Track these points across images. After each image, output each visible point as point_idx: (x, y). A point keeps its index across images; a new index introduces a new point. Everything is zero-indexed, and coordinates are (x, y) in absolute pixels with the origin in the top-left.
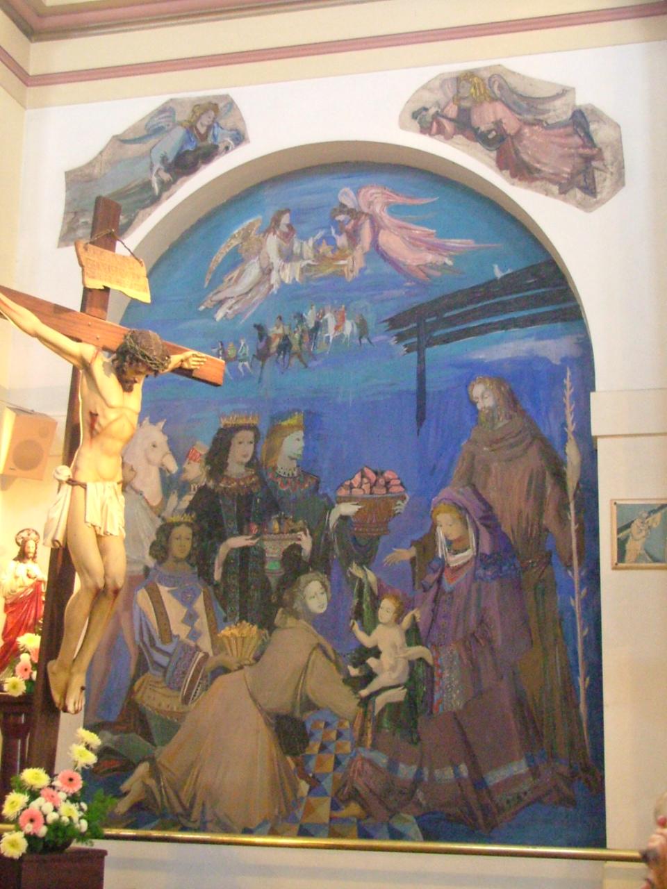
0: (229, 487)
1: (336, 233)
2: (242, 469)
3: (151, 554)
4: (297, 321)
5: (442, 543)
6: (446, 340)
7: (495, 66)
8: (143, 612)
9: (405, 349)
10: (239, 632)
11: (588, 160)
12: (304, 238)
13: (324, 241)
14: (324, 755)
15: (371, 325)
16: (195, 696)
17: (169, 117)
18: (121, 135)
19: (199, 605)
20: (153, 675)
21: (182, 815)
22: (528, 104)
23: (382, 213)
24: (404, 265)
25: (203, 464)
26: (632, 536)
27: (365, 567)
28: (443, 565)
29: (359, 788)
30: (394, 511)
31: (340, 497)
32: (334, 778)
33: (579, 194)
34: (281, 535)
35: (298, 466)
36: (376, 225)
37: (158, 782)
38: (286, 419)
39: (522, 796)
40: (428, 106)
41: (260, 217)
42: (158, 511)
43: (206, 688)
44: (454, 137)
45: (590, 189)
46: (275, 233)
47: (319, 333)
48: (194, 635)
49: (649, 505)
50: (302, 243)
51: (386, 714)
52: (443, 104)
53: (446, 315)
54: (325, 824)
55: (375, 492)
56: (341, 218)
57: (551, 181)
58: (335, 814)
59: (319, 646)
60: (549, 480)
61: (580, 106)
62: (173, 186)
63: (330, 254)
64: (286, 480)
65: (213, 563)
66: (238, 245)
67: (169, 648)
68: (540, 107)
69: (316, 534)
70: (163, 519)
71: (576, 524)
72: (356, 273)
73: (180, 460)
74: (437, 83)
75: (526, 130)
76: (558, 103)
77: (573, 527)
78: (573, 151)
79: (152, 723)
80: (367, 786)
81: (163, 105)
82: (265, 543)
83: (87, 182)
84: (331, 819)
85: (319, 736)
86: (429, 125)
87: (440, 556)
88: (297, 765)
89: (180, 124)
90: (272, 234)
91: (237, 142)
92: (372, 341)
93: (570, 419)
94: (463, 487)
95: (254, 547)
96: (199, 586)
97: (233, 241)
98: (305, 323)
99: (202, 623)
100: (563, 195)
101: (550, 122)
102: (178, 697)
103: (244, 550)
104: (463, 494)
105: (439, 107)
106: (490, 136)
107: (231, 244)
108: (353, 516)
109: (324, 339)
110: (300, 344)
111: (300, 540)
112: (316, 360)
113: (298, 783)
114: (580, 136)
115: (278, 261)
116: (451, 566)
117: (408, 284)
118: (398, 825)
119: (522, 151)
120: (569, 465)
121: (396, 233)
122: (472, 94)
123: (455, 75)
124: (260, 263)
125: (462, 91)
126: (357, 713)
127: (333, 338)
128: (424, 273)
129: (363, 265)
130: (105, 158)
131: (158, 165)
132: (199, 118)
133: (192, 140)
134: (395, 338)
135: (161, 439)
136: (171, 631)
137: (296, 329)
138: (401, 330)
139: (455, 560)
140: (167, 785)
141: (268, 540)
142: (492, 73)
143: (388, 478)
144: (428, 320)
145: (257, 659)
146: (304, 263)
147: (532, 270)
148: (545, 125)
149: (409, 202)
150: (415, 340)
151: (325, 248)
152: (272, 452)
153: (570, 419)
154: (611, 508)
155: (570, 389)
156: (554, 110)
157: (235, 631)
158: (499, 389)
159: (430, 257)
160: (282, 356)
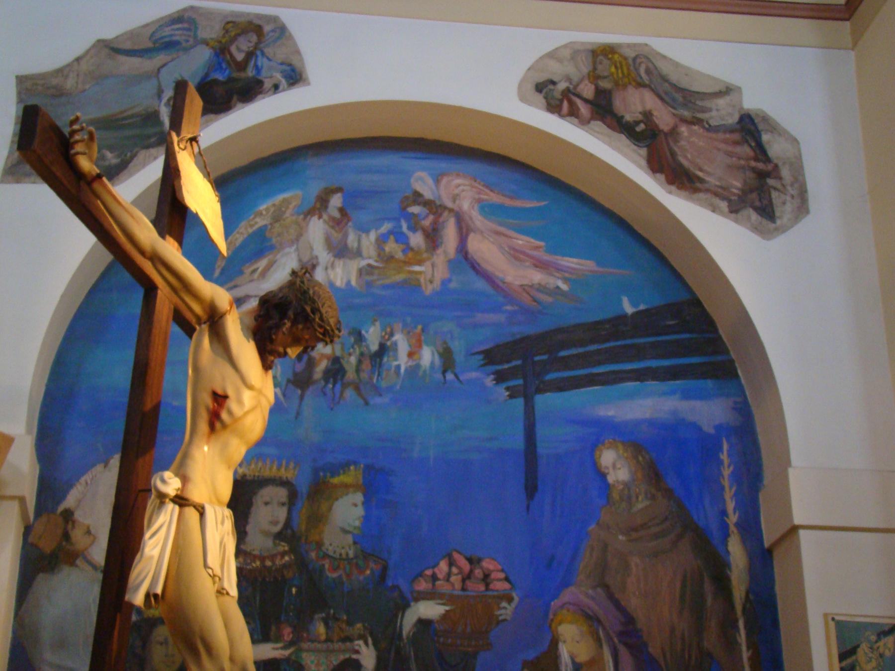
0: (248, 567)
1: (409, 228)
2: (269, 543)
4: (352, 340)
5: (567, 666)
6: (562, 386)
7: (640, 45)
9: (507, 393)
11: (762, 175)
12: (364, 229)
13: (392, 237)
15: (459, 357)
18: (111, 41)
22: (684, 97)
23: (472, 211)
24: (504, 283)
26: (860, 665)
30: (498, 616)
31: (419, 592)
33: (754, 216)
34: (329, 643)
35: (355, 543)
36: (464, 225)
38: (338, 474)
40: (555, 80)
41: (299, 192)
44: (592, 122)
45: (767, 212)
46: (320, 217)
47: (385, 359)
49: (878, 624)
52: (575, 79)
53: (563, 353)
55: (469, 588)
56: (415, 209)
57: (716, 194)
60: (708, 587)
61: (748, 110)
63: (399, 255)
64: (337, 561)
66: (266, 226)
68: (699, 103)
74: (567, 53)
75: (684, 129)
76: (721, 102)
78: (742, 162)
81: (178, 12)
82: (304, 655)
83: (53, 96)
86: (558, 103)
89: (206, 43)
91: (291, 81)
92: (461, 378)
93: (730, 506)
94: (594, 588)
95: (287, 660)
97: (258, 220)
98: (364, 344)
100: (733, 215)
101: (713, 123)
104: (593, 599)
105: (571, 83)
107: (256, 223)
108: (437, 621)
109: (393, 369)
110: (358, 370)
111: (357, 652)
112: (381, 395)
114: (750, 146)
117: (509, 308)
119: (679, 153)
121: (492, 240)
122: (612, 74)
123: (590, 47)
124: (298, 255)
125: (600, 67)
127: (406, 370)
128: (530, 295)
129: (447, 275)
130: (84, 66)
132: (233, 40)
133: (224, 66)
134: (492, 377)
137: (351, 350)
138: (499, 367)
141: (308, 651)
142: (637, 53)
143: (488, 570)
144: (537, 358)
146: (364, 263)
147: (674, 309)
148: (707, 126)
149: (507, 202)
150: (520, 382)
151: (391, 247)
152: (317, 519)
153: (730, 506)
156: (718, 110)
158: (636, 458)
159: (537, 277)
160: (330, 386)
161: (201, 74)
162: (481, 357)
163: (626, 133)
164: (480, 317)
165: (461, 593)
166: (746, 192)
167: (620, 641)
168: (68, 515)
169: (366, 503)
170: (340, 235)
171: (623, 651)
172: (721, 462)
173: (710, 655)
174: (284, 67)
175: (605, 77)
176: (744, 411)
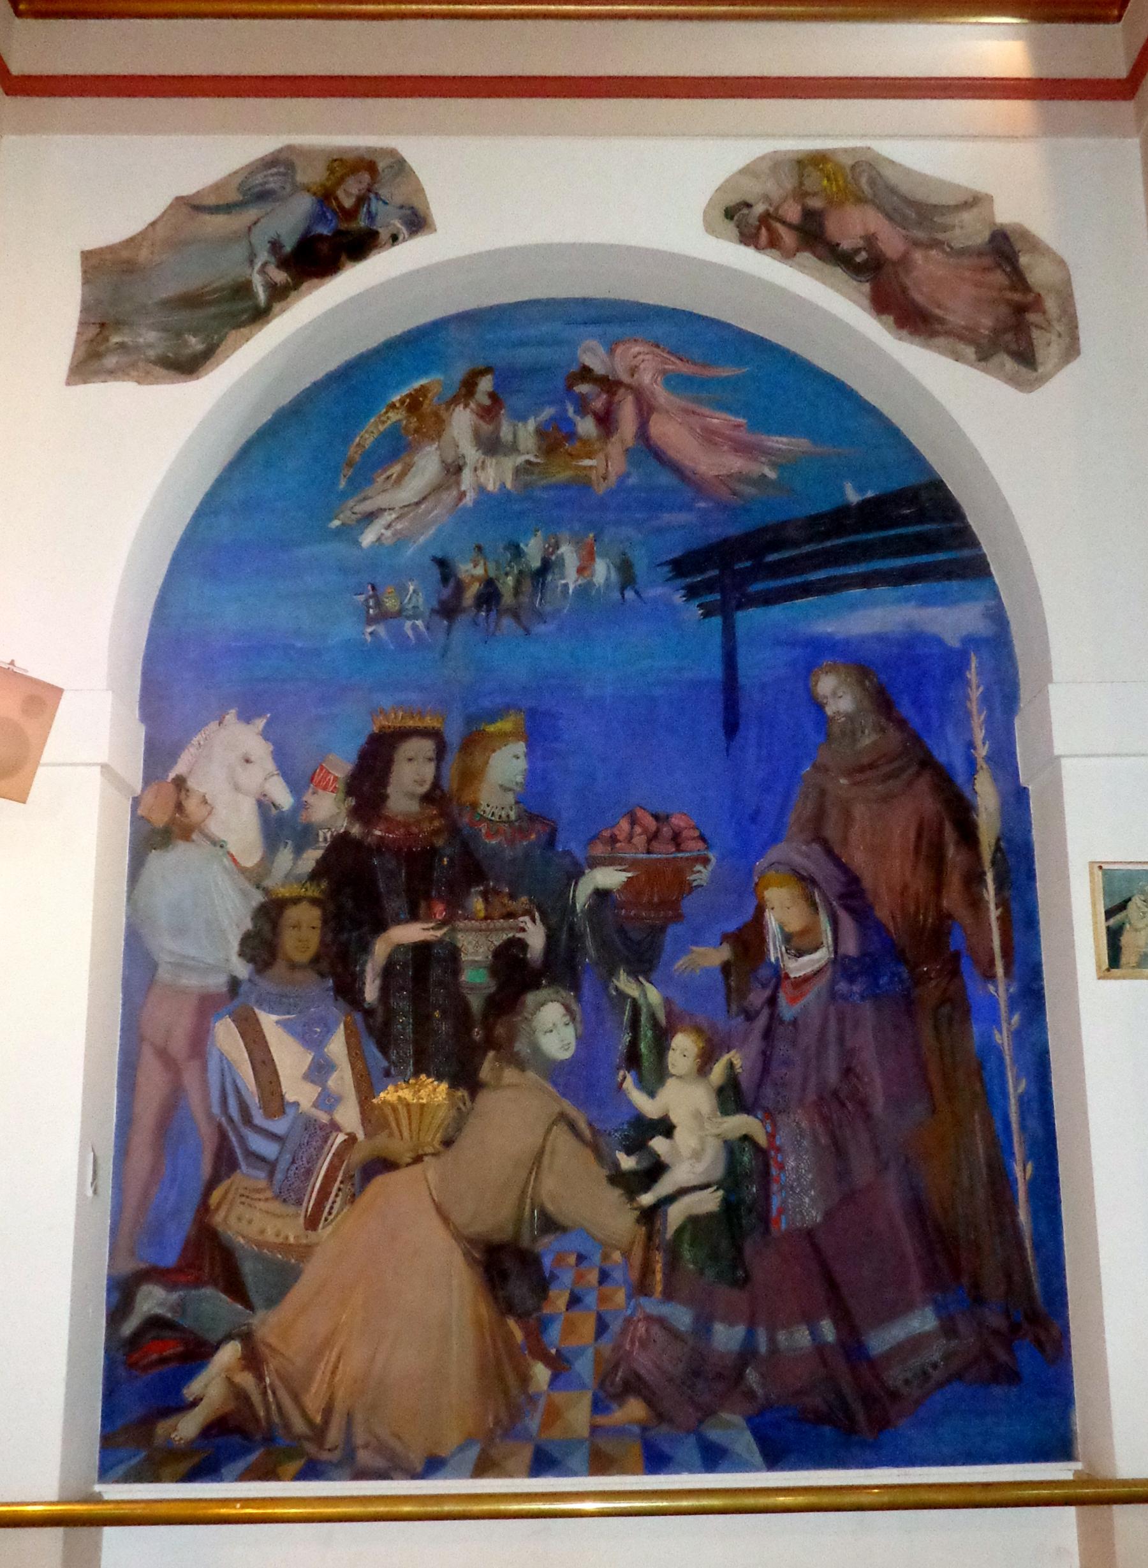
2: (414, 807)
3: (241, 954)
5: (775, 936)
6: (768, 599)
8: (228, 1062)
10: (413, 1095)
11: (1020, 310)
12: (521, 417)
14: (575, 1314)
15: (641, 566)
16: (330, 1213)
17: (284, 175)
19: (337, 1046)
20: (247, 1177)
21: (307, 1438)
25: (341, 795)
27: (641, 978)
28: (779, 976)
29: (642, 1372)
31: (594, 858)
32: (597, 1353)
33: (1010, 364)
35: (517, 803)
37: (260, 1378)
39: (930, 1370)
40: (750, 201)
42: (257, 877)
43: (353, 1198)
44: (798, 254)
45: (1026, 357)
46: (466, 406)
47: (549, 578)
48: (328, 1101)
50: (515, 426)
51: (687, 1237)
53: (772, 558)
54: (581, 1442)
56: (583, 388)
57: (961, 338)
58: (601, 1420)
59: (563, 1117)
60: (950, 834)
61: (1002, 225)
62: (293, 294)
64: (495, 826)
65: (363, 971)
66: (400, 421)
67: (279, 1126)
69: (554, 920)
70: (266, 891)
71: (997, 908)
72: (613, 479)
73: (296, 787)
75: (918, 256)
76: (966, 216)
77: (994, 913)
79: (248, 1268)
80: (658, 1368)
81: (272, 154)
82: (459, 936)
84: (594, 1429)
85: (567, 1278)
86: (754, 231)
87: (773, 959)
88: (527, 1335)
90: (462, 406)
91: (414, 229)
93: (979, 734)
94: (808, 843)
95: (440, 941)
96: (335, 1011)
99: (343, 1080)
100: (983, 364)
101: (957, 245)
102: (298, 1215)
103: (422, 950)
104: (808, 857)
105: (771, 205)
106: (858, 259)
108: (618, 890)
110: (517, 592)
111: (523, 930)
113: (529, 1366)
115: (473, 452)
116: (792, 976)
117: (702, 505)
118: (714, 1434)
120: (982, 809)
126: (635, 1237)
127: (575, 589)
130: (160, 231)
131: (263, 256)
132: (341, 180)
134: (682, 592)
135: (260, 749)
136: (282, 1097)
139: (798, 967)
140: (278, 1383)
141: (466, 930)
142: (856, 161)
145: (448, 1143)
146: (520, 459)
150: (718, 596)
152: (470, 776)
153: (979, 734)
154: (1091, 874)
155: (978, 687)
157: (406, 1094)
159: (736, 464)
161: (301, 228)
162: (666, 569)
163: (842, 266)
164: (666, 517)
165: (645, 856)
166: (997, 332)
167: (841, 905)
168: (180, 783)
169: (530, 754)
170: (491, 427)
171: (847, 923)
172: (967, 683)
173: (950, 916)
174: (404, 211)
175: (815, 194)
176: (998, 618)
